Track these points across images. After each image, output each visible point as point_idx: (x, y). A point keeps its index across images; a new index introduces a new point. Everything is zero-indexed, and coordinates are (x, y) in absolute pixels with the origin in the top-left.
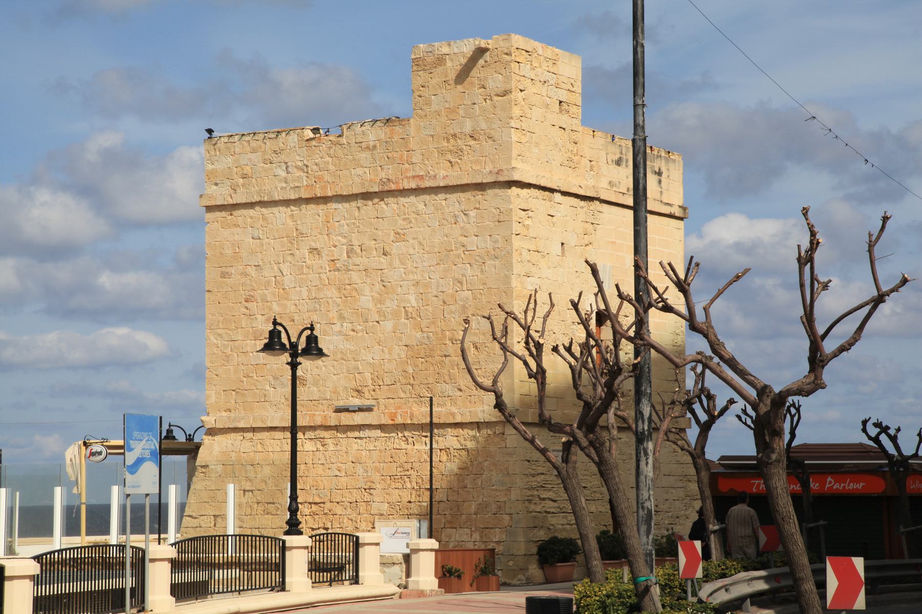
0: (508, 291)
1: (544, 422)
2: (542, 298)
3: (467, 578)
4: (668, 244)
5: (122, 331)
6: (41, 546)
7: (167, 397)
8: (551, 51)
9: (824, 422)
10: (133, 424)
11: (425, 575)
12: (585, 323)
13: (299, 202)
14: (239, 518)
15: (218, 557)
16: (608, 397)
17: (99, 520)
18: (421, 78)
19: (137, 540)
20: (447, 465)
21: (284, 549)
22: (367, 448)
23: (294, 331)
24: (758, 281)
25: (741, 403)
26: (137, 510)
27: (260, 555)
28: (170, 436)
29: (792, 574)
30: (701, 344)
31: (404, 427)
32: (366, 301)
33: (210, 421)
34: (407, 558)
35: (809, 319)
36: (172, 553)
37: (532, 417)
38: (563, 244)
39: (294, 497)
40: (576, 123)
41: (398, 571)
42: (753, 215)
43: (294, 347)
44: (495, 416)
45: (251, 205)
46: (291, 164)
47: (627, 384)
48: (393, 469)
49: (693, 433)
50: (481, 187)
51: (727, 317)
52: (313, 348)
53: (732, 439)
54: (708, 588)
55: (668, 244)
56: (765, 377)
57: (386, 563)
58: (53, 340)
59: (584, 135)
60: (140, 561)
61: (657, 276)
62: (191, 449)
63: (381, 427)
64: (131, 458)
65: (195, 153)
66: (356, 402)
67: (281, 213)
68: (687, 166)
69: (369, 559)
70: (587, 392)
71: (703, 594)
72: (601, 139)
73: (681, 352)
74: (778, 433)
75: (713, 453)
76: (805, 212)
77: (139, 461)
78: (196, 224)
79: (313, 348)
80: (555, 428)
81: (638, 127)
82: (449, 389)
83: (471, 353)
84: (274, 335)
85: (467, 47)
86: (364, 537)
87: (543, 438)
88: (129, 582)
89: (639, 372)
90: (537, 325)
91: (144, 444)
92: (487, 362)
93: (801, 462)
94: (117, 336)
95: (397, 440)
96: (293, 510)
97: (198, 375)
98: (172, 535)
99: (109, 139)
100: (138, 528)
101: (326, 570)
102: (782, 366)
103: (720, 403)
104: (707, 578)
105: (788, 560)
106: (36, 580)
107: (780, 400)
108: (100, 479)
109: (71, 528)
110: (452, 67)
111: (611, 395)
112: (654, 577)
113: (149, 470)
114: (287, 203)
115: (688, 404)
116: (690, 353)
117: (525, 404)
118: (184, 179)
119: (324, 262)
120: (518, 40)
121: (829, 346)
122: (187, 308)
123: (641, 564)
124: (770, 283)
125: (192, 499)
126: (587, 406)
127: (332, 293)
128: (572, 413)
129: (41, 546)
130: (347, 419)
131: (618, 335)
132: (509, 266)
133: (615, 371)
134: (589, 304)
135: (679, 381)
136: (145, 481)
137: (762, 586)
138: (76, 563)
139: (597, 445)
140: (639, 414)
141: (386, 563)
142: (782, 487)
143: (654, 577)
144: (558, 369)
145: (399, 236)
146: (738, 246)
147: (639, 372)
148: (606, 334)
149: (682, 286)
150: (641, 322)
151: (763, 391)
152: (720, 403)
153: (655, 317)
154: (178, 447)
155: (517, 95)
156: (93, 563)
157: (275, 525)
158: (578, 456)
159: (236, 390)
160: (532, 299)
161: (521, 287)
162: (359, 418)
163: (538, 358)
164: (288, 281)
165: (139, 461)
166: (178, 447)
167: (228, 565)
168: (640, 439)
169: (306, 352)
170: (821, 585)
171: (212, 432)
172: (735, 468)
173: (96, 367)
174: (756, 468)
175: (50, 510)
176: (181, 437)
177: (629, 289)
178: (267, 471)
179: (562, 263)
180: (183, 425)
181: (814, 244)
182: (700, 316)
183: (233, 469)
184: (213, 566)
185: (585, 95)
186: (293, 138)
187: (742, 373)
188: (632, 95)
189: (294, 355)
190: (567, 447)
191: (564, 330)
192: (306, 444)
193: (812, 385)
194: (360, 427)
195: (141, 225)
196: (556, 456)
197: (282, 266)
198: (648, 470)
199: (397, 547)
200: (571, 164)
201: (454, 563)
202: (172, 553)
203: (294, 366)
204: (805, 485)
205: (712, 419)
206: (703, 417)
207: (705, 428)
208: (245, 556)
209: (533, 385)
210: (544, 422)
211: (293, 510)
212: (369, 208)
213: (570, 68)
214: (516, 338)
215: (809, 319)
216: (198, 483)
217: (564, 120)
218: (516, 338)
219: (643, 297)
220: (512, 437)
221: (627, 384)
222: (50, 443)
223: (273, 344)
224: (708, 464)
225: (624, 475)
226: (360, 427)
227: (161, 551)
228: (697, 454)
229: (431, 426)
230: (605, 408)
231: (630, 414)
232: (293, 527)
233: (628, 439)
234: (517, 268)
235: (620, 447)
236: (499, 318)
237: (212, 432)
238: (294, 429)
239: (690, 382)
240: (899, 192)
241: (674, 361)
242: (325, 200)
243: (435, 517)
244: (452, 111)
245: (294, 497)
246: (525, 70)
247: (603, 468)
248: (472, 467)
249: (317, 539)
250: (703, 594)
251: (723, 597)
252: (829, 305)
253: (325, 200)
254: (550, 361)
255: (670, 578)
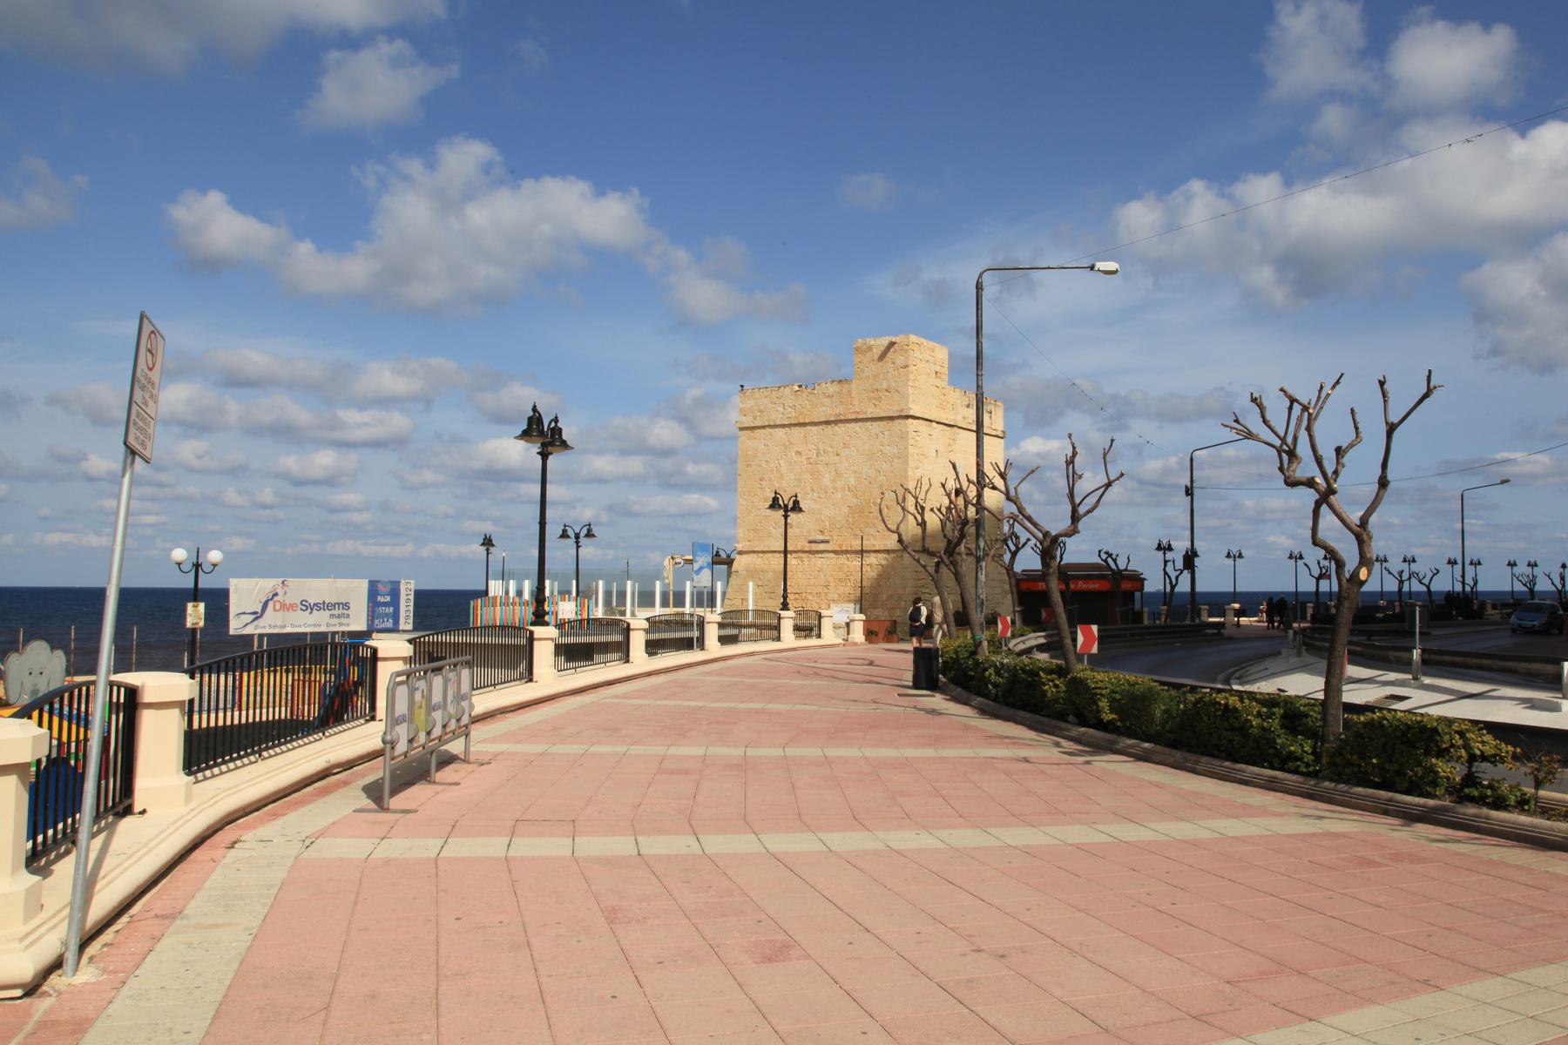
0: (906, 477)
1: (925, 550)
2: (925, 481)
3: (881, 636)
4: (995, 452)
5: (696, 496)
6: (648, 613)
7: (717, 534)
8: (931, 344)
9: (1078, 551)
10: (697, 548)
11: (858, 634)
12: (948, 495)
13: (790, 425)
14: (755, 601)
15: (743, 621)
16: (960, 539)
17: (679, 600)
18: (859, 357)
19: (699, 611)
20: (870, 573)
21: (780, 618)
22: (826, 563)
23: (786, 498)
24: (1048, 474)
25: (1034, 541)
26: (700, 594)
27: (767, 621)
28: (718, 554)
29: (1059, 634)
30: (1013, 509)
31: (846, 552)
32: (826, 481)
33: (739, 547)
34: (848, 625)
35: (1071, 495)
36: (719, 619)
37: (918, 547)
38: (1382, 384)
39: (785, 590)
40: (944, 384)
41: (843, 631)
42: (1047, 437)
43: (786, 506)
44: (897, 546)
45: (763, 427)
46: (786, 405)
47: (971, 530)
48: (842, 576)
49: (1007, 557)
50: (891, 418)
51: (1026, 490)
52: (796, 507)
53: (1029, 560)
54: (1014, 642)
55: (995, 452)
56: (1047, 527)
57: (836, 627)
58: (660, 500)
59: (950, 390)
60: (701, 624)
61: (988, 470)
62: (729, 562)
63: (834, 552)
64: (696, 566)
65: (737, 399)
66: (821, 537)
67: (780, 432)
68: (1006, 410)
69: (826, 625)
70: (949, 534)
71: (1011, 645)
72: (958, 393)
73: (1001, 511)
74: (1054, 558)
75: (1018, 568)
76: (1070, 436)
77: (701, 568)
78: (736, 438)
79: (796, 507)
80: (932, 554)
81: (979, 387)
82: (872, 531)
83: (885, 511)
84: (775, 500)
85: (885, 341)
86: (824, 612)
87: (924, 559)
88: (696, 634)
89: (978, 523)
90: (922, 496)
91: (703, 559)
92: (894, 516)
93: (1066, 573)
94: (693, 499)
95: (842, 559)
96: (785, 597)
97: (734, 521)
98: (719, 609)
99: (695, 392)
100: (700, 604)
101: (802, 630)
102: (1056, 521)
103: (1023, 540)
104: (1013, 636)
105: (1057, 627)
106: (647, 631)
107: (1055, 540)
108: (680, 577)
109: (665, 604)
110: (877, 352)
111: (963, 536)
112: (984, 636)
113: (706, 573)
114: (783, 426)
115: (1005, 541)
116: (1006, 513)
117: (914, 540)
118: (735, 414)
119: (803, 459)
120: (913, 338)
121: (1082, 510)
122: (728, 486)
123: (977, 629)
124: (1054, 474)
125: (730, 589)
126: (949, 541)
127: (807, 476)
128: (941, 545)
129: (648, 613)
130: (815, 547)
131: (967, 503)
132: (906, 462)
133: (965, 522)
134: (951, 485)
135: (1000, 528)
136: (704, 579)
137: (1043, 641)
138: (668, 622)
139: (954, 564)
140: (978, 547)
141: (836, 627)
142: (1055, 586)
143: (984, 636)
144: (933, 521)
145: (846, 446)
146: (1038, 454)
147: (978, 523)
148: (960, 501)
149: (1003, 476)
150: (979, 496)
151: (1046, 534)
152: (1023, 540)
153: (987, 492)
154: (723, 561)
155: (912, 368)
156: (677, 623)
157: (775, 604)
158: (944, 569)
159: (754, 530)
160: (919, 482)
161: (913, 475)
162: (822, 547)
163: (922, 515)
164: (784, 469)
165: (701, 568)
166: (723, 561)
167: (749, 626)
168: (978, 560)
169: (793, 509)
170: (1075, 640)
171: (740, 553)
172: (1029, 576)
173: (682, 516)
174: (1043, 576)
175: (653, 593)
176: (723, 555)
177: (974, 478)
178: (771, 575)
179: (937, 463)
180: (725, 549)
181: (1075, 454)
182: (1012, 493)
183: (752, 574)
184: (740, 626)
185: (950, 368)
186: (788, 390)
187: (1035, 525)
188: (976, 371)
189: (786, 511)
190: (937, 564)
191: (938, 499)
192: (792, 560)
193: (1072, 531)
194: (822, 552)
195: (713, 438)
196: (931, 570)
197: (781, 462)
198: (982, 578)
199: (842, 619)
200: (942, 407)
201: (874, 628)
202: (719, 619)
203: (786, 517)
204: (1067, 585)
205: (1018, 549)
206: (1013, 548)
207: (1014, 554)
208: (758, 622)
209: (919, 530)
210: (925, 550)
211: (785, 597)
212: (829, 429)
213: (942, 353)
214: (910, 504)
215: (1071, 495)
216: (733, 581)
217: (938, 382)
218: (910, 504)
219: (981, 481)
220: (907, 559)
221: (971, 530)
222: (655, 557)
223: (775, 505)
224: (1015, 574)
225: (969, 581)
226: (822, 552)
227: (713, 617)
228: (1009, 569)
229: (862, 552)
230: (959, 543)
231: (973, 546)
232: (785, 606)
233: (972, 560)
234: (911, 464)
235: (967, 565)
236: (901, 492)
237: (740, 553)
238: (785, 552)
239: (1006, 528)
240: (1124, 428)
241: (998, 517)
242: (804, 424)
243: (864, 602)
244: (876, 376)
245: (785, 590)
246: (917, 354)
247: (958, 576)
248: (884, 575)
249: (798, 613)
250: (1011, 645)
251: (1022, 647)
252: (1083, 487)
253: (804, 424)
254: (928, 516)
255: (993, 636)
